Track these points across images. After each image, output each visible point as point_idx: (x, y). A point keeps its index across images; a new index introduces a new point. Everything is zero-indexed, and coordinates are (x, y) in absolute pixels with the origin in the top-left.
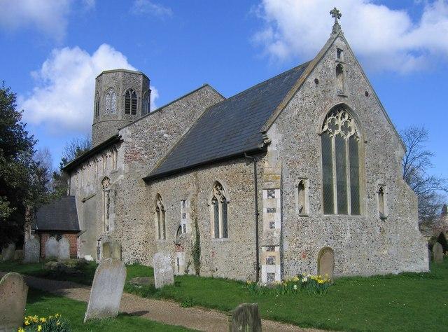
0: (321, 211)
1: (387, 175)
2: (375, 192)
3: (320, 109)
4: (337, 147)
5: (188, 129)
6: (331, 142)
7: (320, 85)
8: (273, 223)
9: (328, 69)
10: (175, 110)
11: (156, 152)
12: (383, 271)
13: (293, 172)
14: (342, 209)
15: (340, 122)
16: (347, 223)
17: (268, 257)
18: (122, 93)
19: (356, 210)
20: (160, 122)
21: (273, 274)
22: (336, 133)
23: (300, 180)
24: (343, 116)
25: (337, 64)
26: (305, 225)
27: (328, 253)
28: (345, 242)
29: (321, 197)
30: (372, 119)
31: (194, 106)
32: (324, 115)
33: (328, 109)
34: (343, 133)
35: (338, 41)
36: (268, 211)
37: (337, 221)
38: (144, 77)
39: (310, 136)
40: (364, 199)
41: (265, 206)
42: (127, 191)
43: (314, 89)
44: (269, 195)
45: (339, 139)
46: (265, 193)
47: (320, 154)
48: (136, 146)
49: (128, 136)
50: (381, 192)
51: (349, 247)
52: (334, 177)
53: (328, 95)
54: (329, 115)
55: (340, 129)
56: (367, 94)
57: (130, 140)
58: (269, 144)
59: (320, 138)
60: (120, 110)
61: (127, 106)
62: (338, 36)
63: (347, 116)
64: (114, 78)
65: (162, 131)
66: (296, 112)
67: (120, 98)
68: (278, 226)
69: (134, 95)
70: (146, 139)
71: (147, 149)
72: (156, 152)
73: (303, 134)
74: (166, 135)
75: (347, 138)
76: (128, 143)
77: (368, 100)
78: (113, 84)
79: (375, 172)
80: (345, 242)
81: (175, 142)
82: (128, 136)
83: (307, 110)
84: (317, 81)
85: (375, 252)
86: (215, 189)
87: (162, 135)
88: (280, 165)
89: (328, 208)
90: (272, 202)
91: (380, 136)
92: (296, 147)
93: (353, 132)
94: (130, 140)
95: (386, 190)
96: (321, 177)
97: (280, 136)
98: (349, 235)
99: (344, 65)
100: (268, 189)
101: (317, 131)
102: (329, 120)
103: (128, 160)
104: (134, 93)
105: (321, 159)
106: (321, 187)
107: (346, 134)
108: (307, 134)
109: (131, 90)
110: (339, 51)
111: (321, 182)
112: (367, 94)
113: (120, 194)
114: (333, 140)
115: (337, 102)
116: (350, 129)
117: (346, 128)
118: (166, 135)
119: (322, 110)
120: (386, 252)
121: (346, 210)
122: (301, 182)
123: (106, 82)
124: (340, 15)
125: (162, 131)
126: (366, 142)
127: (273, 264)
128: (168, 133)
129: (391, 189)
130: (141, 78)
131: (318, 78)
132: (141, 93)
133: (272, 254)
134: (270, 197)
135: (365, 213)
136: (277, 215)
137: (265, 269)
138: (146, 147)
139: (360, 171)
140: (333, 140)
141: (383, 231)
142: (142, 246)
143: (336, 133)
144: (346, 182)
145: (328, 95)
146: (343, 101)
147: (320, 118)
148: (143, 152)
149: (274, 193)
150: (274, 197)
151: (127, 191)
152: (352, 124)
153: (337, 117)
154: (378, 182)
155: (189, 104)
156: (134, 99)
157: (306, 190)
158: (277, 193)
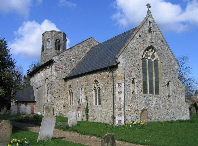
0: (142, 93)
1: (171, 77)
2: (166, 84)
3: (142, 48)
4: (149, 65)
5: (83, 57)
6: (146, 63)
7: (141, 37)
8: (121, 98)
9: (145, 30)
10: (77, 48)
11: (69, 67)
12: (169, 119)
13: (130, 75)
14: (151, 92)
15: (150, 54)
16: (153, 98)
17: (118, 113)
18: (54, 41)
19: (157, 92)
20: (71, 54)
21: (121, 120)
22: (149, 58)
23: (132, 79)
24: (152, 51)
25: (149, 28)
26: (135, 99)
27: (145, 111)
28: (152, 106)
29: (142, 86)
30: (164, 52)
31: (86, 47)
32: (143, 51)
33: (145, 48)
34: (151, 59)
35: (149, 18)
36: (118, 93)
37: (149, 97)
38: (64, 34)
39: (137, 60)
40: (161, 88)
41: (117, 91)
42: (56, 84)
43: (139, 39)
44: (119, 86)
45: (150, 61)
46: (117, 85)
47: (141, 68)
48: (60, 64)
49: (57, 60)
50: (168, 84)
51: (154, 108)
52: (148, 78)
53: (145, 42)
54: (145, 50)
55: (150, 57)
56: (162, 41)
57: (57, 62)
58: (119, 63)
59: (141, 61)
60: (53, 48)
61: (56, 47)
62: (149, 16)
63: (153, 51)
64: (50, 34)
65: (72, 58)
66: (131, 49)
67: (53, 43)
68: (123, 99)
69: (59, 42)
70: (64, 61)
71: (65, 66)
72: (69, 67)
73: (134, 59)
74: (73, 60)
75: (153, 61)
76: (56, 63)
77: (163, 44)
78: (50, 37)
79: (166, 76)
80: (152, 106)
81: (77, 62)
82: (57, 60)
83: (136, 48)
84: (140, 36)
85: (166, 111)
86: (95, 83)
87: (72, 59)
88: (124, 72)
89: (145, 92)
90: (120, 89)
91: (168, 60)
92: (131, 65)
93: (156, 58)
94: (57, 62)
95: (171, 83)
96: (142, 78)
97: (124, 60)
98: (154, 104)
99: (152, 29)
100: (118, 83)
101: (140, 58)
102: (145, 53)
103: (56, 70)
104: (59, 41)
105: (142, 70)
106: (142, 82)
107: (153, 59)
108: (136, 59)
109: (58, 40)
110: (150, 23)
111: (142, 80)
112: (162, 41)
113: (53, 85)
114: (147, 62)
115: (149, 45)
116: (155, 57)
117: (153, 56)
118: (73, 60)
119: (142, 49)
120: (170, 111)
121: (153, 92)
122: (133, 80)
123: (47, 36)
124: (150, 7)
125: (72, 58)
126: (162, 63)
127: (120, 116)
128: (74, 59)
129: (173, 83)
130: (62, 34)
131: (141, 34)
132: (62, 41)
133: (120, 112)
134: (119, 87)
135: (161, 94)
136: (123, 95)
137: (117, 118)
138: (65, 65)
139: (159, 75)
140: (147, 62)
141: (169, 102)
142: (63, 108)
143: (149, 58)
144: (153, 80)
145: (145, 42)
146: (152, 44)
147: (141, 52)
148: (63, 67)
149: (121, 85)
150: (121, 87)
151: (56, 84)
152: (156, 54)
153: (149, 52)
154: (167, 80)
155: (83, 46)
156: (59, 43)
157: (135, 83)
158: (123, 85)
